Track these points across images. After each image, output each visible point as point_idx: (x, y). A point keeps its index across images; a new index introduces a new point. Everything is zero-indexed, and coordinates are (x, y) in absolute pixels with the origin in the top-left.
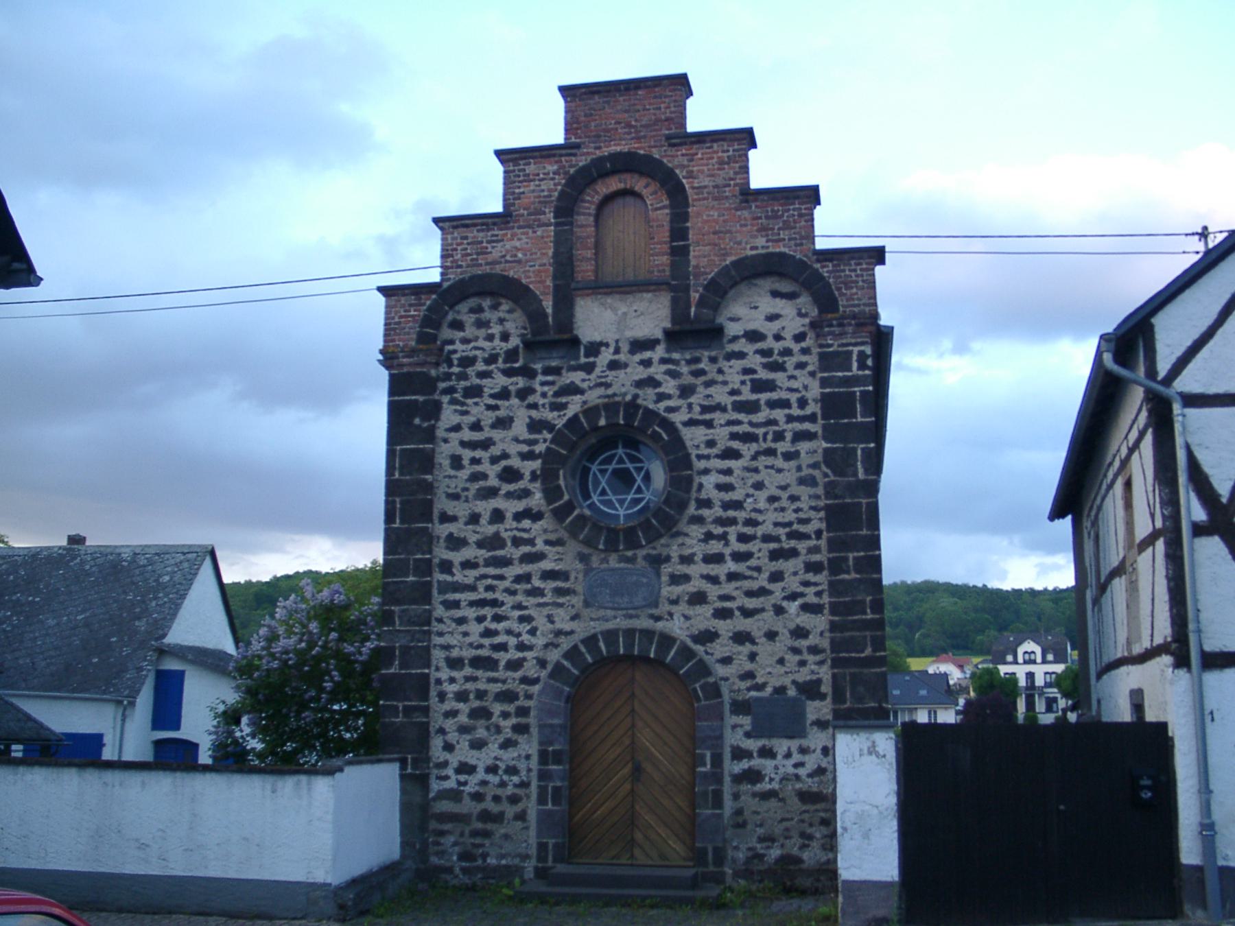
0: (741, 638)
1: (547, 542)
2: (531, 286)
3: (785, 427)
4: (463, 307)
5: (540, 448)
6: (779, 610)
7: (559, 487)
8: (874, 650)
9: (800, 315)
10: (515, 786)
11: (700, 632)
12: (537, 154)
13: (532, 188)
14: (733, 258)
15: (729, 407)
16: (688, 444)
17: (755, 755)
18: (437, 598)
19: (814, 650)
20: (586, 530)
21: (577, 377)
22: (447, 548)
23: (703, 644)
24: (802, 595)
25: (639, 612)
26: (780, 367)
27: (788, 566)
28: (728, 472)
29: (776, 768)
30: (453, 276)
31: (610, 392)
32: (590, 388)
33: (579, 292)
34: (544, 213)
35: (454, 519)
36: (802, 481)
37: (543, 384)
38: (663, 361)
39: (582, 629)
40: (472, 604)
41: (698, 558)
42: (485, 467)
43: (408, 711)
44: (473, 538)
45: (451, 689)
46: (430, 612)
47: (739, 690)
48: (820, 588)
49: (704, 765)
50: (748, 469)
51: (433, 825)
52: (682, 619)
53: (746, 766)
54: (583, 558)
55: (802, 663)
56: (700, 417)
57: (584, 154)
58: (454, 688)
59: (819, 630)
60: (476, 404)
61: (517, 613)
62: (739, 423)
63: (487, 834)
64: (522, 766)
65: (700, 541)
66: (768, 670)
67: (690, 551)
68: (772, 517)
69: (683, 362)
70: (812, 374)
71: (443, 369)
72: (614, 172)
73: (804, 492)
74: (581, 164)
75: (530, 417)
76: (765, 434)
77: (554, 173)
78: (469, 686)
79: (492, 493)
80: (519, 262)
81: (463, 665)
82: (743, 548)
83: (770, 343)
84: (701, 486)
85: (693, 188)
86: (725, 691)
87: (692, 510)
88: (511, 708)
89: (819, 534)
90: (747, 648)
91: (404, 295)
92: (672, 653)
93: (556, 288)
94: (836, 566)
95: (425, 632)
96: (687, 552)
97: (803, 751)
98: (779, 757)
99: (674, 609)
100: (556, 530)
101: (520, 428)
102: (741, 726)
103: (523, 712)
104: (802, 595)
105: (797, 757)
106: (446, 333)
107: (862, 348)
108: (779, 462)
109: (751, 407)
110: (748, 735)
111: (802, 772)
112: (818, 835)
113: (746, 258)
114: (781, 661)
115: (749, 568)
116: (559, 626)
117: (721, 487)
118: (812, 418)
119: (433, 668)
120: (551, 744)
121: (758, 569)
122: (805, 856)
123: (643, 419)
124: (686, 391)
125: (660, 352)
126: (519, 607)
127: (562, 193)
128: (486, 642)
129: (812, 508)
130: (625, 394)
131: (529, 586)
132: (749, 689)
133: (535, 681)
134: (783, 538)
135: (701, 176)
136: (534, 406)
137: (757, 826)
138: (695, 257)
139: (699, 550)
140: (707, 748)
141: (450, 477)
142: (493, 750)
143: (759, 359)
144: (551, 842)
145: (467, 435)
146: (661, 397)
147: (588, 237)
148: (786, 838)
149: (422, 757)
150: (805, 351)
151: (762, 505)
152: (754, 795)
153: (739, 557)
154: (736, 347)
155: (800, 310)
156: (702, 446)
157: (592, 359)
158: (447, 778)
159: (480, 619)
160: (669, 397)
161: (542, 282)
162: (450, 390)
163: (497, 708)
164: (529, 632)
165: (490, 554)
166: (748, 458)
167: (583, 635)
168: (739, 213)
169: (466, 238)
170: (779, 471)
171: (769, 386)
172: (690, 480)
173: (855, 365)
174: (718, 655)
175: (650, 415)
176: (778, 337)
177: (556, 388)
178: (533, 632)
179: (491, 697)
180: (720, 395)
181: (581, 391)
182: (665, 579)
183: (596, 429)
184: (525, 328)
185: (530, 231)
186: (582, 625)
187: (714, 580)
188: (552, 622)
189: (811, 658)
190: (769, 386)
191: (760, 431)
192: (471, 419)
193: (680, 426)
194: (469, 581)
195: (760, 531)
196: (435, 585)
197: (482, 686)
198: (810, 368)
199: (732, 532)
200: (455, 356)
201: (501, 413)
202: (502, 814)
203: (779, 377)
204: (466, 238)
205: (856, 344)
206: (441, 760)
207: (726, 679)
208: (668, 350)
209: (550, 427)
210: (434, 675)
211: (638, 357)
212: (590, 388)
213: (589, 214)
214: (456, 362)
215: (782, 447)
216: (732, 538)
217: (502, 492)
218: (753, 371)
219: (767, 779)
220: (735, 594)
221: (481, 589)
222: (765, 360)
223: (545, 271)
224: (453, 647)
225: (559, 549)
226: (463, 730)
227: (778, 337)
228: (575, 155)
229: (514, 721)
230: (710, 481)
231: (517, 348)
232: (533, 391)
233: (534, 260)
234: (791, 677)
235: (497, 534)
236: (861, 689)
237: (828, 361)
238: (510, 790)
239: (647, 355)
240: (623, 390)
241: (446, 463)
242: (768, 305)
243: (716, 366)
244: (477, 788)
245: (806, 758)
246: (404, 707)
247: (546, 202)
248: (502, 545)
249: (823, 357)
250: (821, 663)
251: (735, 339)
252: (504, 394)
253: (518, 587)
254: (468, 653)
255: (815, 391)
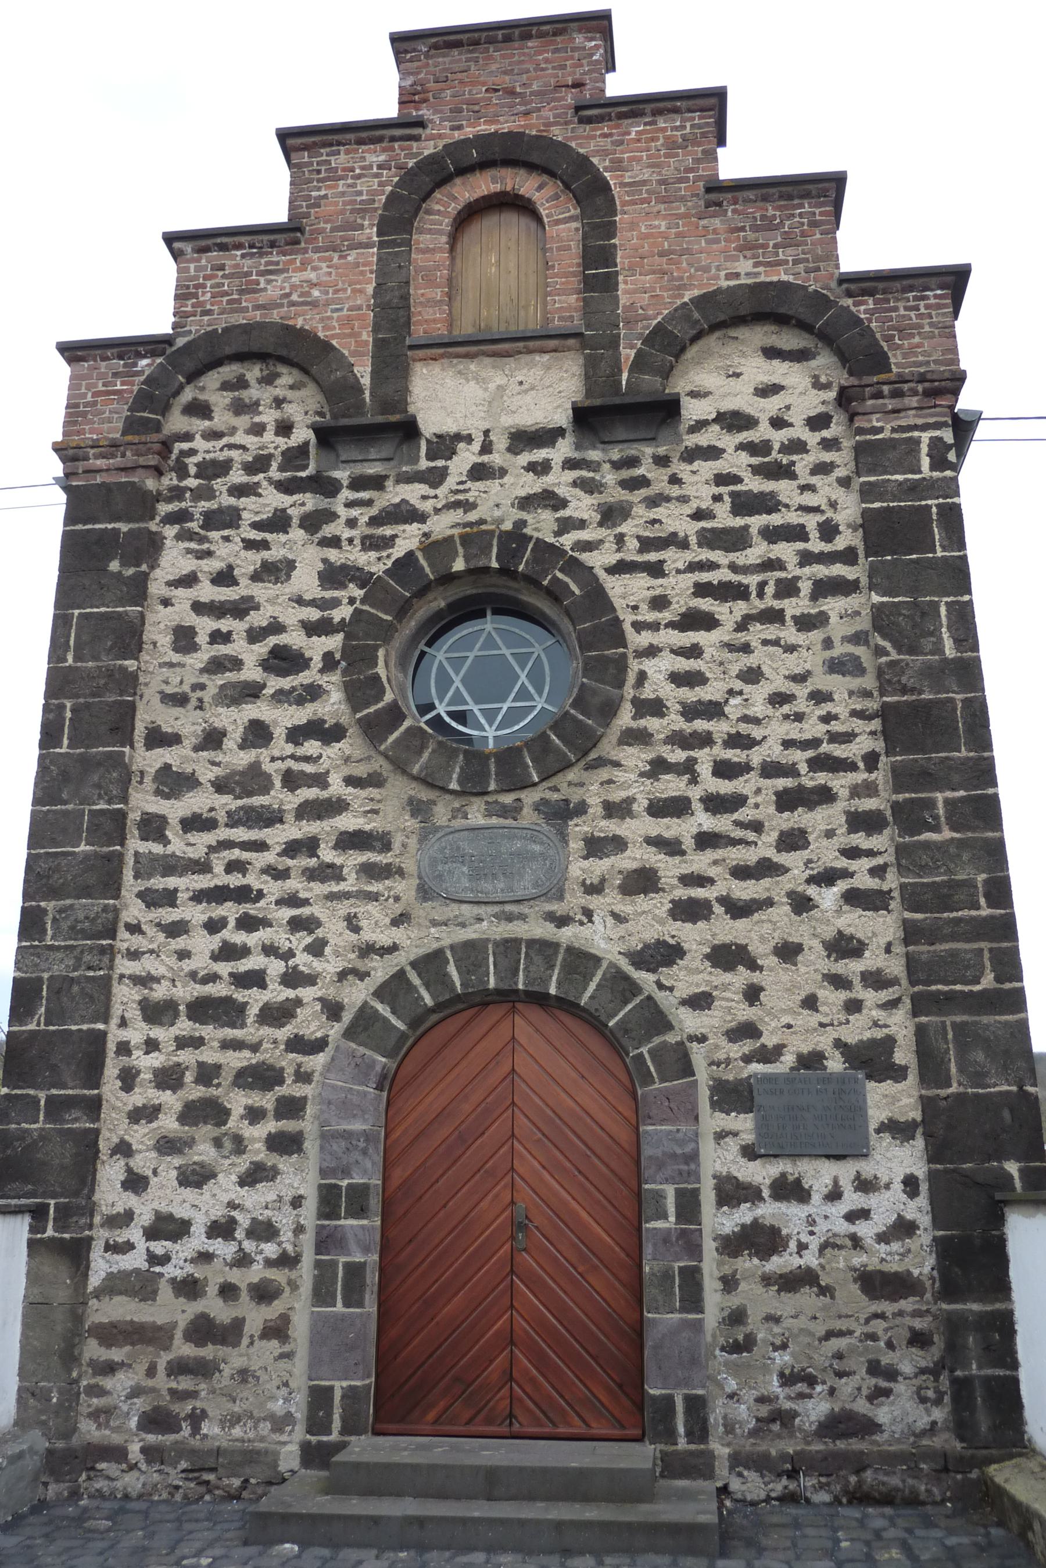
0: (727, 956)
1: (351, 781)
2: (334, 342)
3: (798, 572)
4: (212, 380)
5: (342, 613)
6: (802, 904)
7: (377, 678)
8: (998, 979)
9: (818, 385)
10: (269, 1263)
11: (647, 946)
12: (351, 136)
13: (340, 189)
14: (696, 292)
15: (693, 540)
16: (618, 603)
17: (766, 1193)
18: (130, 885)
19: (875, 980)
20: (426, 755)
21: (413, 493)
22: (158, 792)
23: (654, 971)
24: (846, 874)
25: (524, 909)
26: (786, 472)
27: (813, 820)
28: (694, 652)
29: (811, 1221)
30: (196, 327)
31: (473, 516)
32: (437, 511)
33: (420, 353)
34: (361, 227)
35: (173, 740)
36: (835, 666)
37: (349, 505)
38: (570, 464)
39: (413, 943)
40: (199, 897)
41: (640, 806)
42: (239, 647)
43: (57, 1107)
44: (207, 774)
45: (147, 1063)
46: (116, 911)
47: (728, 1061)
48: (880, 860)
49: (665, 1217)
50: (730, 647)
51: (93, 1350)
52: (610, 921)
53: (748, 1219)
54: (418, 809)
55: (854, 1006)
56: (639, 558)
57: (432, 138)
58: (156, 1060)
59: (883, 941)
60: (227, 539)
61: (287, 913)
62: (712, 566)
63: (203, 1369)
64: (284, 1220)
65: (642, 774)
66: (786, 1019)
67: (623, 794)
68: (777, 730)
69: (607, 466)
70: (845, 483)
71: (170, 480)
72: (484, 165)
73: (839, 685)
74: (426, 153)
75: (325, 561)
76: (762, 585)
77: (380, 167)
78: (187, 1057)
79: (251, 692)
80: (314, 304)
81: (176, 1015)
82: (725, 787)
83: (764, 431)
84: (642, 677)
85: (623, 185)
86: (698, 1055)
87: (625, 718)
88: (267, 1101)
89: (871, 760)
90: (741, 977)
91: (104, 359)
92: (592, 986)
93: (380, 345)
94: (910, 817)
95: (103, 951)
96: (617, 795)
97: (865, 1185)
98: (816, 1198)
99: (594, 902)
100: (369, 758)
101: (305, 580)
102: (735, 1134)
103: (291, 1108)
104: (846, 874)
105: (852, 1199)
106: (176, 422)
107: (937, 433)
108: (790, 634)
109: (735, 540)
110: (749, 1153)
111: (865, 1230)
112: (906, 1368)
113: (719, 291)
114: (810, 1003)
115: (738, 824)
116: (368, 935)
117: (678, 679)
118: (848, 556)
119: (114, 1021)
120: (346, 1173)
121: (757, 827)
122: (883, 1414)
123: (535, 559)
124: (611, 515)
125: (563, 449)
126: (292, 900)
127: (392, 198)
128: (224, 969)
129: (854, 713)
130: (500, 521)
131: (313, 862)
132: (747, 1059)
133: (318, 1045)
134: (803, 768)
135: (637, 168)
136: (334, 542)
137: (776, 1348)
138: (626, 292)
139: (642, 792)
140: (667, 1181)
141: (171, 665)
142: (226, 1187)
143: (745, 459)
144: (339, 1386)
145: (207, 592)
146: (566, 526)
147: (437, 268)
148: (840, 1375)
149: (79, 1202)
150: (829, 444)
151: (759, 709)
152: (767, 1280)
153: (716, 804)
154: (702, 439)
155: (816, 377)
156: (644, 607)
157: (440, 463)
158: (128, 1247)
159: (213, 926)
160: (582, 524)
161: (355, 335)
162: (180, 517)
163: (238, 1101)
164: (308, 949)
165: (240, 803)
166: (730, 626)
167: (415, 953)
168: (702, 222)
169: (222, 268)
170: (791, 649)
171: (767, 504)
172: (621, 665)
173: (925, 462)
174: (684, 990)
175: (547, 552)
176: (778, 423)
177: (374, 511)
178: (317, 949)
179: (226, 1078)
180: (675, 520)
181: (420, 517)
182: (576, 845)
183: (448, 578)
184: (321, 414)
185: (336, 256)
186: (414, 933)
187: (671, 847)
188: (356, 929)
189: (870, 997)
190: (767, 504)
191: (752, 580)
192: (215, 565)
193: (602, 574)
194: (197, 853)
195: (756, 756)
196: (130, 860)
197: (209, 1055)
198: (840, 472)
199: (705, 759)
200: (191, 461)
201: (274, 554)
202: (238, 1324)
203: (784, 489)
204: (222, 268)
205: (924, 428)
206: (119, 1209)
207: (702, 1039)
208: (578, 447)
209: (363, 578)
210: (115, 1035)
211: (524, 458)
212: (437, 511)
213: (439, 232)
214: (192, 470)
215: (792, 607)
216: (705, 769)
217: (268, 691)
218: (737, 480)
219: (793, 1245)
220: (712, 872)
221: (219, 868)
222: (756, 461)
223: (360, 318)
224: (157, 980)
225: (373, 792)
226: (167, 1146)
227: (778, 423)
228: (417, 138)
229: (271, 1126)
230: (658, 668)
231: (306, 444)
232: (332, 516)
233: (340, 301)
234: (832, 1034)
235: (255, 768)
236: (980, 1056)
237: (869, 455)
238: (256, 1273)
239: (540, 454)
240: (497, 513)
241: (165, 640)
242: (760, 370)
243: (669, 471)
244: (190, 1269)
245: (871, 1201)
246: (49, 1099)
247: (364, 211)
248: (265, 788)
249: (859, 450)
250: (891, 1005)
251: (700, 425)
252: (279, 522)
253: (290, 862)
254: (186, 992)
255: (849, 509)
